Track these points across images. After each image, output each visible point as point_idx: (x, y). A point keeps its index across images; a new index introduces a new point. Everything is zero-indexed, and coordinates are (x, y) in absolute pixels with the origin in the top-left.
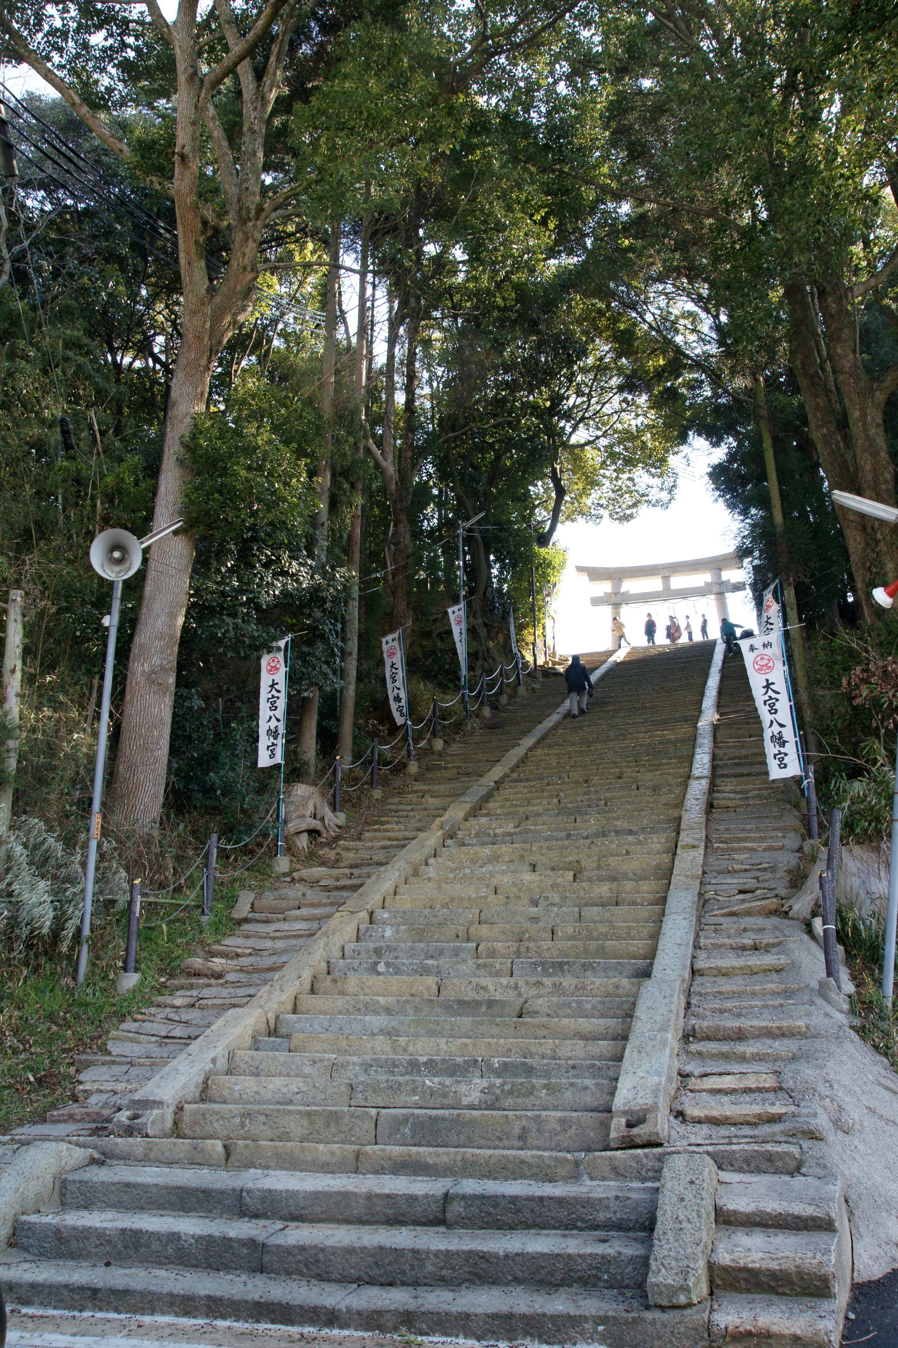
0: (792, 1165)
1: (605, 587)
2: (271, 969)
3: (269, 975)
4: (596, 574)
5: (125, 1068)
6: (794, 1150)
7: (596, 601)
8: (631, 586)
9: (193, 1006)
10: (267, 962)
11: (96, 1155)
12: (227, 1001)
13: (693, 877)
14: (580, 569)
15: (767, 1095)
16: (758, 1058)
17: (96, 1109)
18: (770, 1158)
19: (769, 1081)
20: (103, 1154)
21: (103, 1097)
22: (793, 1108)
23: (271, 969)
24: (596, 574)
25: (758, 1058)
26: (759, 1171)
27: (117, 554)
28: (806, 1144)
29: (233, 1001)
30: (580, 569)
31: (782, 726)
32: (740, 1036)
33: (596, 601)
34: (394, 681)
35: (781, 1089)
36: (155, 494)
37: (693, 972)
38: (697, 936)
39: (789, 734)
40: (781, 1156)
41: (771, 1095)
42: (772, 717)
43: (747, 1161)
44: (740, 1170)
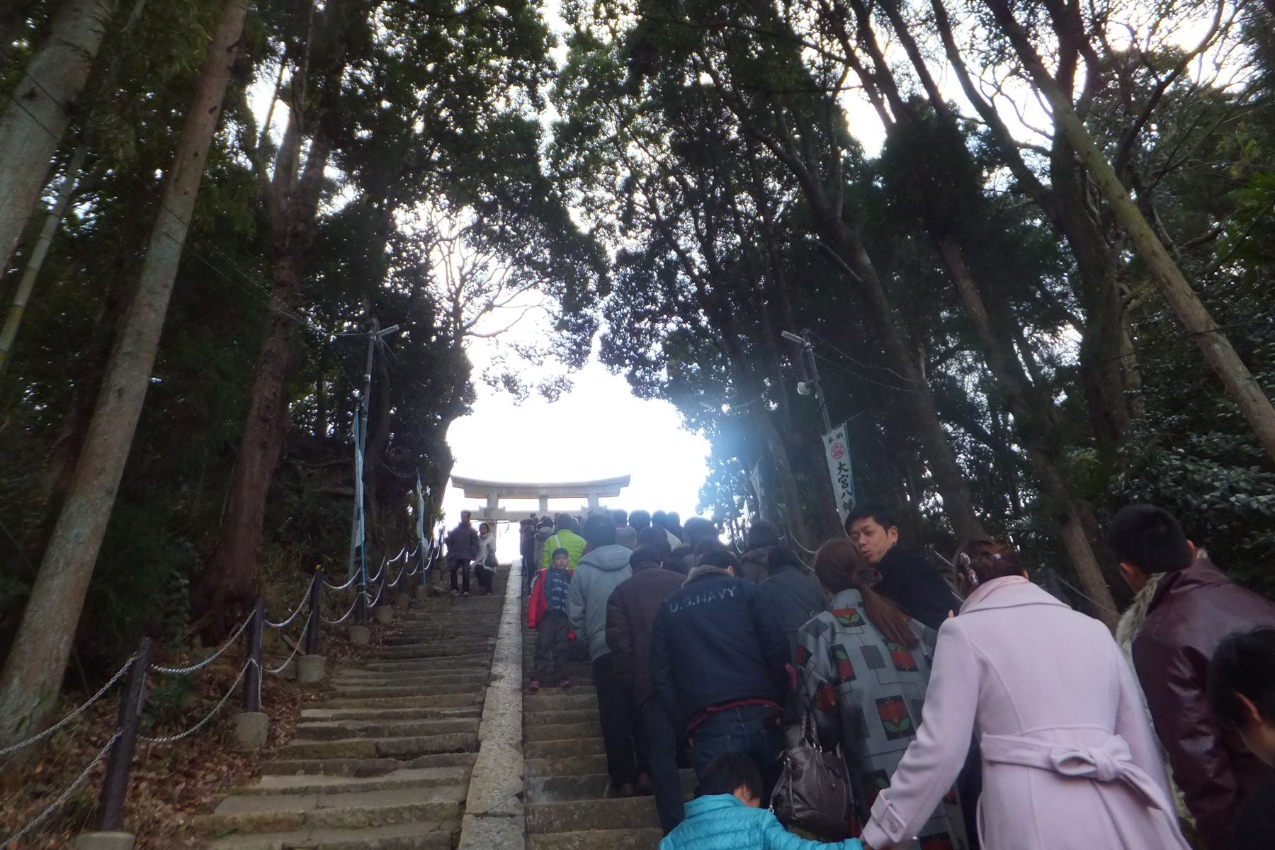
8: (507, 504)
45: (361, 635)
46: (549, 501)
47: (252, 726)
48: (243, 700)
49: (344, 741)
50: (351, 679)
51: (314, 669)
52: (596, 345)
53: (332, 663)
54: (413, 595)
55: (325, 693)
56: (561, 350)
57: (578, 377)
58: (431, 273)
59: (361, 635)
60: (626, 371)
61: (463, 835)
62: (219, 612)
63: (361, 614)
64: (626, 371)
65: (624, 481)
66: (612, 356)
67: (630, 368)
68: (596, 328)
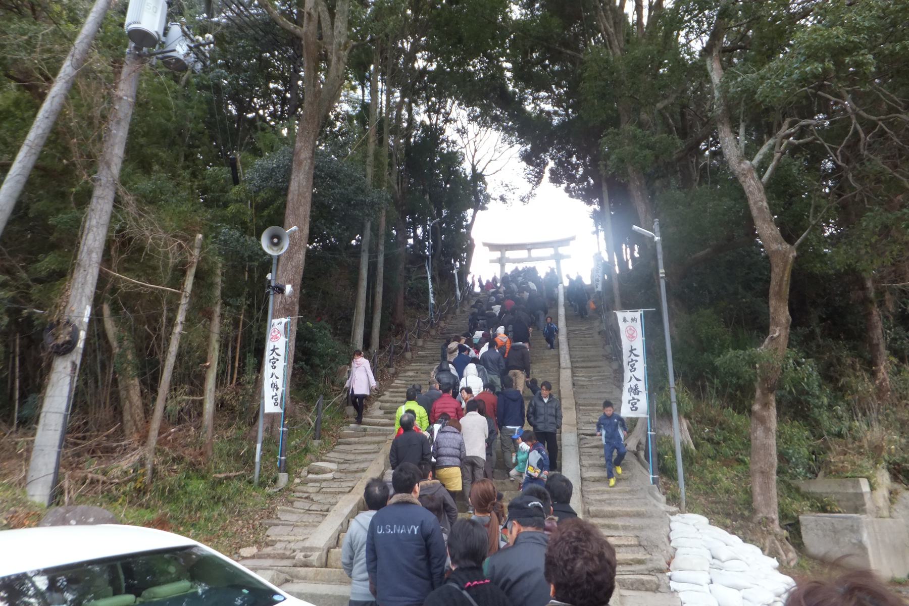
0: (654, 587)
1: (497, 254)
2: (356, 471)
3: (358, 475)
4: (493, 247)
5: (291, 528)
6: (654, 578)
7: (492, 261)
8: (510, 254)
9: (318, 492)
10: (354, 467)
11: (288, 578)
12: (338, 490)
13: (573, 425)
14: (485, 244)
15: (633, 548)
16: (625, 528)
17: (282, 552)
18: (642, 583)
19: (633, 541)
20: (292, 576)
21: (283, 545)
22: (648, 556)
23: (356, 471)
24: (493, 247)
25: (625, 528)
26: (638, 589)
27: (275, 240)
28: (660, 575)
29: (340, 490)
30: (485, 244)
31: (638, 380)
32: (613, 515)
33: (492, 261)
34: (633, 369)
35: (640, 545)
36: (285, 207)
37: (582, 479)
38: (580, 459)
39: (642, 386)
40: (649, 582)
41: (636, 549)
42: (631, 374)
43: (632, 585)
44: (628, 589)
45: (433, 332)
46: (533, 251)
47: (408, 355)
48: (406, 350)
49: (257, 459)
50: (429, 345)
51: (420, 343)
52: (547, 174)
53: (425, 341)
54: (454, 313)
55: (423, 348)
56: (530, 176)
57: (539, 190)
58: (466, 167)
59: (433, 332)
60: (564, 186)
61: (563, 402)
62: (400, 329)
63: (432, 326)
64: (564, 186)
65: (573, 238)
66: (556, 178)
67: (565, 185)
68: (547, 164)
